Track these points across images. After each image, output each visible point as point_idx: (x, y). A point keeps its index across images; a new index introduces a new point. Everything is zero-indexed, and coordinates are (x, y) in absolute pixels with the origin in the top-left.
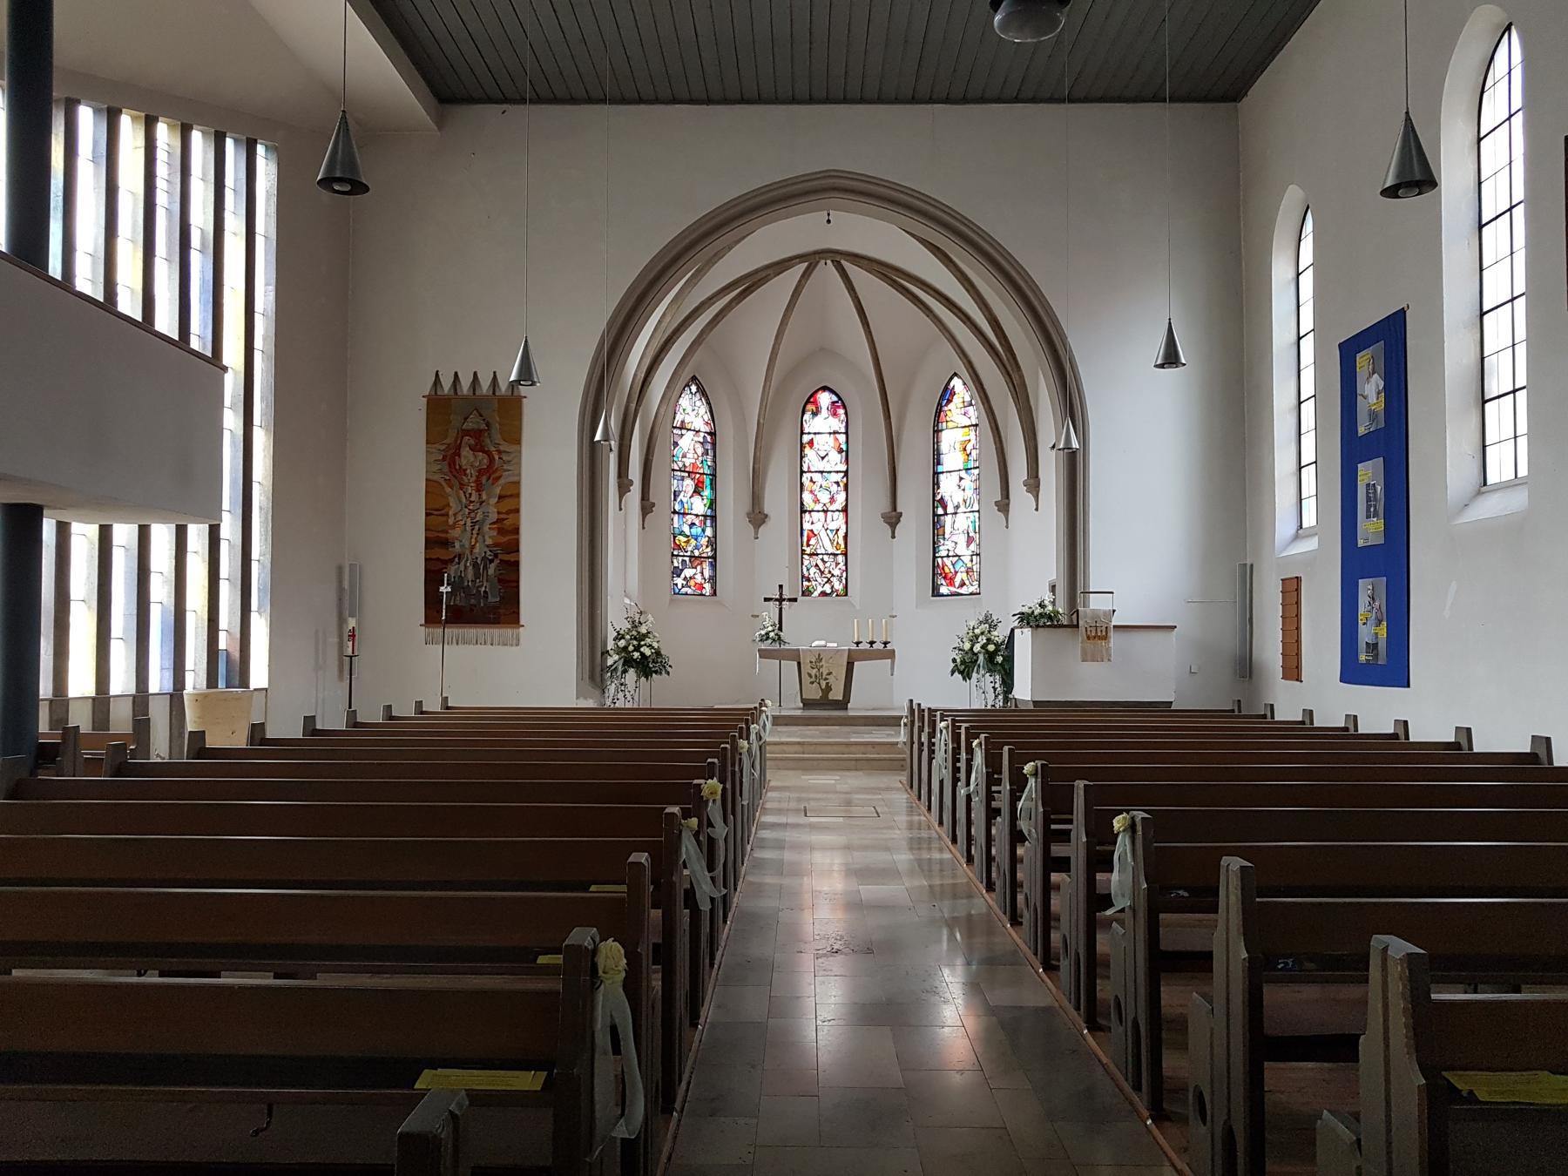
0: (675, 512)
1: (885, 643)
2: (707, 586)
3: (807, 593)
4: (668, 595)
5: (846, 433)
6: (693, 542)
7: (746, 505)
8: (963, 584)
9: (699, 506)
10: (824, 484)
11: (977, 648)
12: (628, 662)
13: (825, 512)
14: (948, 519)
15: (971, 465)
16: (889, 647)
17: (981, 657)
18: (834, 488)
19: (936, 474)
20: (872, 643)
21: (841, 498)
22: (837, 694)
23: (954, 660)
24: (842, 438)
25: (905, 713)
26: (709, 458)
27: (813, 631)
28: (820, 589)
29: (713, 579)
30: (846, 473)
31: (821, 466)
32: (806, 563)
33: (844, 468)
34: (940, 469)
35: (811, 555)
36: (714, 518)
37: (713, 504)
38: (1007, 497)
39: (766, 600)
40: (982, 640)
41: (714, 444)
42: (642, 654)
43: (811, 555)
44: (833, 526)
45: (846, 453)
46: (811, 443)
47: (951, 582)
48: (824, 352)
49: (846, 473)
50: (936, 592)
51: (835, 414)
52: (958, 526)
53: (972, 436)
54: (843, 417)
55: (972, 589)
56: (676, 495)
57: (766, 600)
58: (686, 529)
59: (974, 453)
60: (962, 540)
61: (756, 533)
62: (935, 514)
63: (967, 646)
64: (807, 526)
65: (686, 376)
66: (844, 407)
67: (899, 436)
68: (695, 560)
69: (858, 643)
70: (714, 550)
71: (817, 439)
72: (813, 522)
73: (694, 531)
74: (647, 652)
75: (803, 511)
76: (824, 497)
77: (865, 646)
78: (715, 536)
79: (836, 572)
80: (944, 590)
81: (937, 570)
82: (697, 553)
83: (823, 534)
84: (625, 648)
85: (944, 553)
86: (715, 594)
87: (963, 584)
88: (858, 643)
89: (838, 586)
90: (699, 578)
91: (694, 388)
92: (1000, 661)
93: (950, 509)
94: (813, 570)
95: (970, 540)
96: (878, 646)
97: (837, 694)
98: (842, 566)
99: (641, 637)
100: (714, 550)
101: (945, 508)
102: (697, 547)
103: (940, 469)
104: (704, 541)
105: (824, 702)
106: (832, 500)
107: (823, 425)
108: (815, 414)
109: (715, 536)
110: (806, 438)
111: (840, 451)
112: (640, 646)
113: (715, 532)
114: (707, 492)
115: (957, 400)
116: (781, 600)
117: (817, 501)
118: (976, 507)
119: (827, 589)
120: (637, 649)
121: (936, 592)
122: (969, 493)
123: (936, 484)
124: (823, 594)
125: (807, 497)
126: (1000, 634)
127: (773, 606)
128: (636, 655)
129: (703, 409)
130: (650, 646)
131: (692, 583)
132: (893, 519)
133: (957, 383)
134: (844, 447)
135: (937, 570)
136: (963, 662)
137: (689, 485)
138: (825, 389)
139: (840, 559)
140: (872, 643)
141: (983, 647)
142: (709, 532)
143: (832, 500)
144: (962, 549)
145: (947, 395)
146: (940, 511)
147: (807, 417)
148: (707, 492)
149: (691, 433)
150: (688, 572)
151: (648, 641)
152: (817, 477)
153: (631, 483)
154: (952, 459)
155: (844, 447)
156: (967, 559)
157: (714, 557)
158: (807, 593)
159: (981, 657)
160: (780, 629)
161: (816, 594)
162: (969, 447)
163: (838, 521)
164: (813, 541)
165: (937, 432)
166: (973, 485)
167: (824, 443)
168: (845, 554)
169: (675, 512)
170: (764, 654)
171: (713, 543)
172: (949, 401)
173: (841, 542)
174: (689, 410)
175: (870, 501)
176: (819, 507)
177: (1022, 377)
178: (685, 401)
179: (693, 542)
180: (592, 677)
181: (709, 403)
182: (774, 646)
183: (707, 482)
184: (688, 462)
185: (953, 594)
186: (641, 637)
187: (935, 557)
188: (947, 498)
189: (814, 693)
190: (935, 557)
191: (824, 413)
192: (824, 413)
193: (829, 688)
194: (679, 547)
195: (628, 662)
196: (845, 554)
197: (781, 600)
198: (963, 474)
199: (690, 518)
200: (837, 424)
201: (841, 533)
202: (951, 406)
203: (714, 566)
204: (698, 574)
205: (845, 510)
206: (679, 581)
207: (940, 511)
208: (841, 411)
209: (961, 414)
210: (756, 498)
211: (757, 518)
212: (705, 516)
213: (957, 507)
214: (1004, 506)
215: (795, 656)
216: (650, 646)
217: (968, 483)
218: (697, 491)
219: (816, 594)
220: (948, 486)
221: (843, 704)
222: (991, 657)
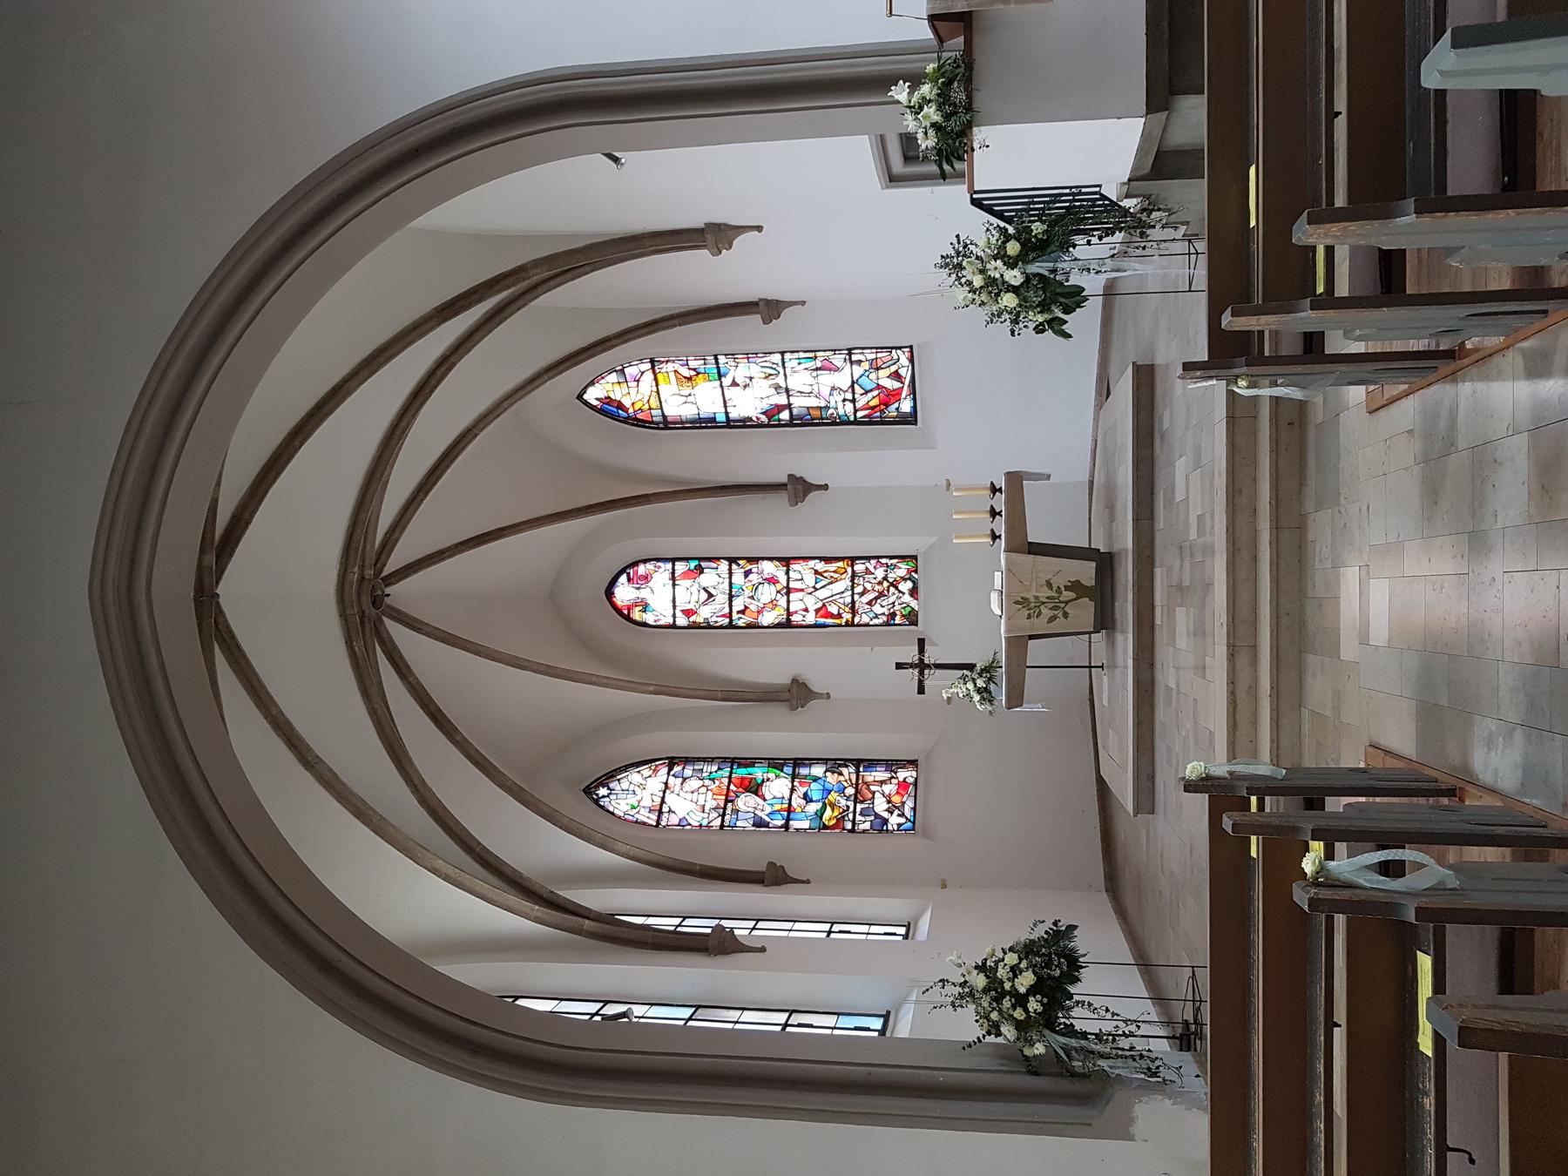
0: (786, 826)
1: (994, 490)
2: (902, 774)
3: (912, 618)
4: (910, 842)
5: (673, 560)
6: (833, 797)
7: (777, 711)
8: (896, 376)
9: (778, 786)
10: (748, 593)
11: (1014, 277)
12: (1048, 1020)
13: (789, 591)
14: (799, 403)
15: (711, 367)
16: (1001, 483)
17: (1033, 268)
18: (754, 578)
19: (730, 423)
20: (994, 513)
21: (769, 568)
22: (1086, 572)
23: (1039, 329)
24: (681, 567)
25: (1216, 388)
26: (707, 768)
27: (976, 609)
28: (907, 598)
29: (892, 765)
30: (732, 561)
31: (722, 598)
32: (865, 619)
33: (724, 565)
34: (721, 418)
35: (854, 611)
36: (798, 763)
37: (776, 764)
38: (755, 304)
39: (921, 690)
40: (996, 268)
41: (687, 761)
42: (1033, 990)
43: (854, 611)
44: (810, 579)
45: (701, 563)
46: (688, 613)
47: (890, 397)
48: (553, 599)
49: (732, 561)
50: (910, 419)
51: (646, 578)
52: (813, 387)
53: (670, 367)
54: (650, 566)
55: (904, 361)
56: (759, 823)
57: (921, 690)
58: (813, 808)
59: (693, 364)
60: (827, 379)
61: (820, 696)
62: (790, 423)
63: (1009, 300)
64: (811, 618)
65: (579, 809)
66: (635, 564)
67: (671, 482)
68: (860, 794)
69: (995, 537)
70: (846, 762)
71: (681, 605)
72: (805, 607)
73: (816, 795)
74: (1025, 981)
75: (788, 624)
76: (767, 593)
77: (1000, 526)
78: (825, 761)
79: (880, 573)
80: (906, 406)
81: (875, 419)
82: (850, 791)
83: (822, 594)
84: (1019, 1025)
85: (849, 407)
86: (913, 763)
87: (896, 376)
88: (995, 537)
89: (902, 571)
90: (887, 788)
91: (603, 791)
92: (1043, 228)
93: (783, 400)
94: (877, 609)
95: (829, 368)
96: (1000, 502)
97: (1086, 572)
98: (871, 565)
99: (995, 989)
100: (846, 762)
101: (780, 408)
102: (842, 791)
103: (721, 418)
104: (832, 778)
105: (1102, 594)
106: (772, 580)
107: (659, 596)
108: (645, 607)
109: (825, 761)
110: (682, 621)
111: (700, 570)
112: (1014, 993)
113: (819, 761)
114: (758, 773)
115: (617, 394)
116: (922, 666)
117: (773, 604)
118: (777, 358)
119: (906, 586)
120: (1021, 1001)
121: (910, 419)
122: (755, 370)
123: (745, 423)
124: (914, 592)
125: (768, 618)
126: (979, 229)
127: (933, 679)
128: (1034, 1005)
129: (635, 776)
130: (1015, 971)
131: (896, 799)
132: (798, 488)
133: (592, 395)
134: (693, 564)
135: (875, 419)
136: (1044, 307)
137: (746, 802)
138: (609, 593)
139: (859, 567)
140: (994, 513)
141: (1011, 263)
142: (818, 770)
143: (772, 580)
144: (843, 380)
145: (610, 409)
146: (785, 415)
147: (649, 618)
148: (758, 773)
149: (669, 798)
150: (880, 806)
151: (1002, 973)
152: (738, 604)
153: (719, 929)
154: (706, 399)
155: (693, 564)
156: (858, 371)
157: (857, 763)
158: (912, 618)
159: (1033, 268)
160: (971, 667)
161: (914, 604)
162: (685, 372)
163: (803, 573)
164: (833, 609)
165: (666, 424)
166: (743, 364)
167: (688, 594)
168: (853, 560)
169: (786, 826)
170: (1015, 698)
171: (835, 765)
172: (620, 406)
173: (833, 567)
174: (633, 800)
175: (770, 527)
176: (783, 601)
177: (536, 263)
178: (620, 805)
179: (833, 797)
180: (1083, 1099)
181: (626, 768)
182: (998, 680)
183: (742, 772)
184: (711, 804)
185: (913, 392)
186: (995, 989)
187: (856, 422)
188: (765, 405)
189: (1083, 612)
190: (856, 422)
191: (644, 594)
192: (644, 594)
193: (1075, 586)
194: (841, 820)
195: (1048, 1020)
196: (853, 560)
197: (922, 666)
198: (727, 381)
199: (797, 802)
200: (661, 575)
201: (820, 566)
202: (627, 402)
203: (871, 764)
204: (883, 790)
205: (786, 562)
206: (894, 820)
207: (785, 415)
208: (642, 569)
209: (634, 388)
210: (767, 695)
211: (797, 694)
212: (794, 777)
213: (777, 387)
214: (770, 309)
215: (1017, 644)
216: (1015, 971)
217: (741, 371)
218: (754, 788)
219: (914, 604)
220: (748, 404)
221: (1105, 562)
222: (1033, 248)
